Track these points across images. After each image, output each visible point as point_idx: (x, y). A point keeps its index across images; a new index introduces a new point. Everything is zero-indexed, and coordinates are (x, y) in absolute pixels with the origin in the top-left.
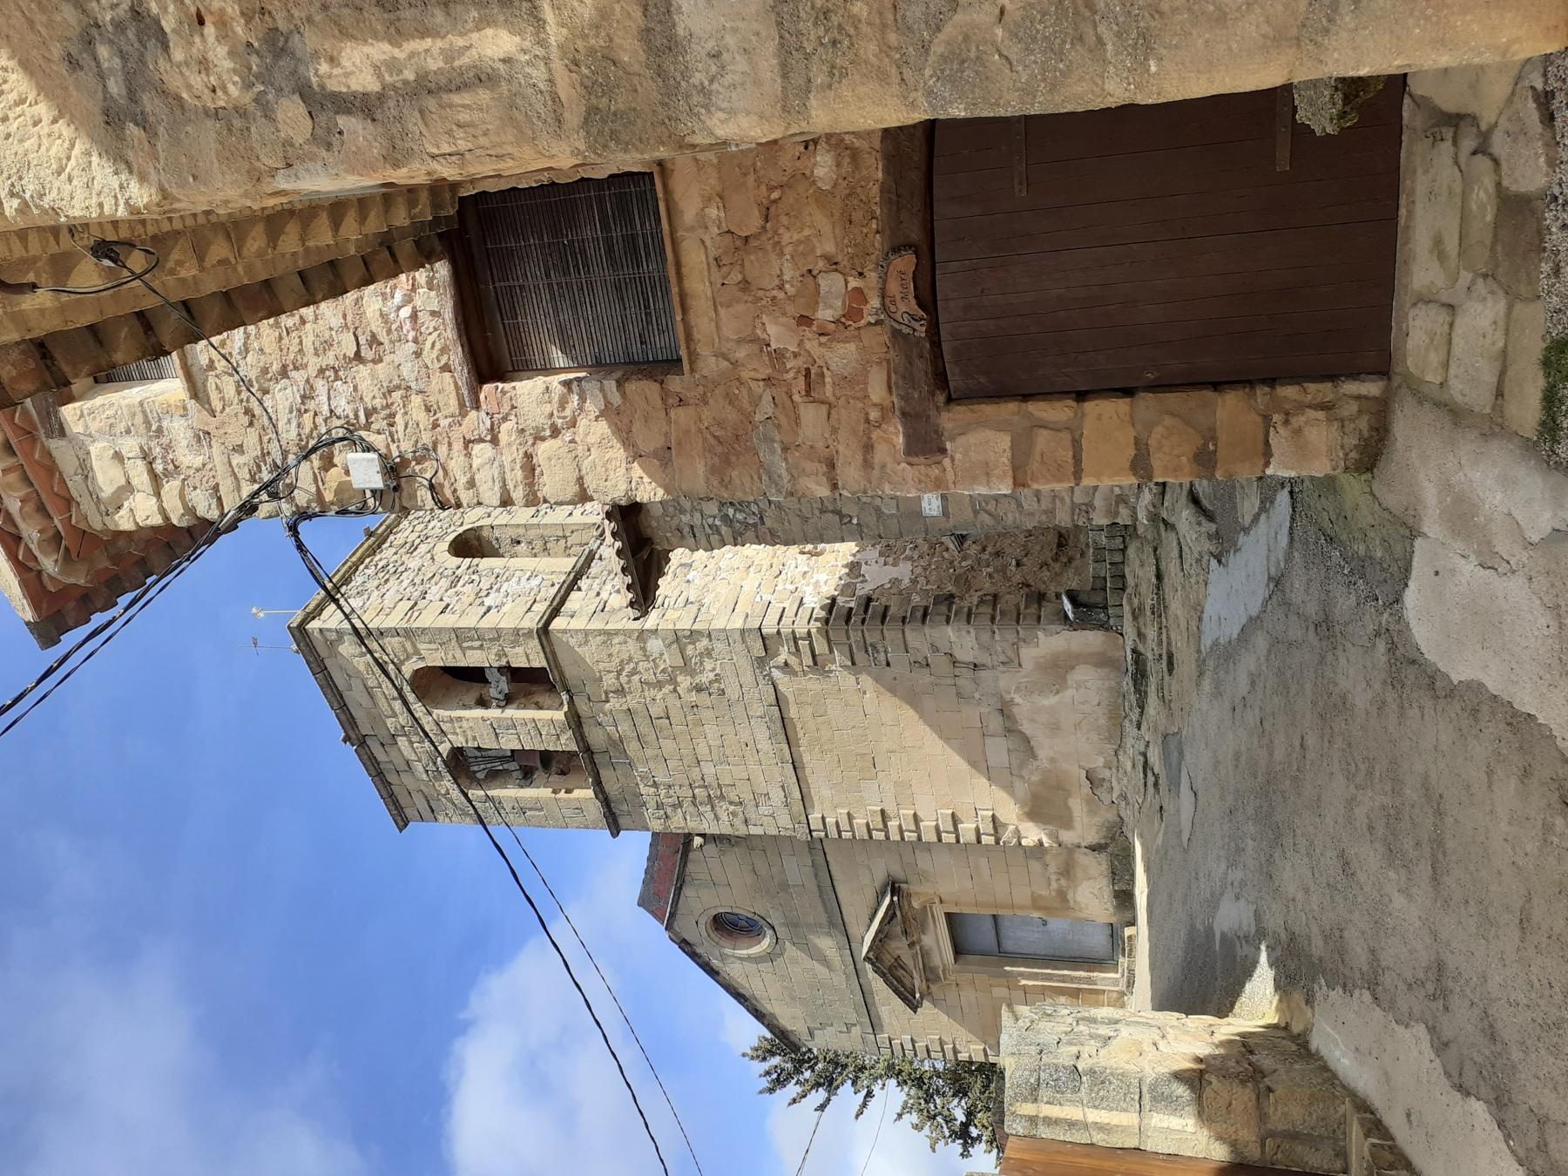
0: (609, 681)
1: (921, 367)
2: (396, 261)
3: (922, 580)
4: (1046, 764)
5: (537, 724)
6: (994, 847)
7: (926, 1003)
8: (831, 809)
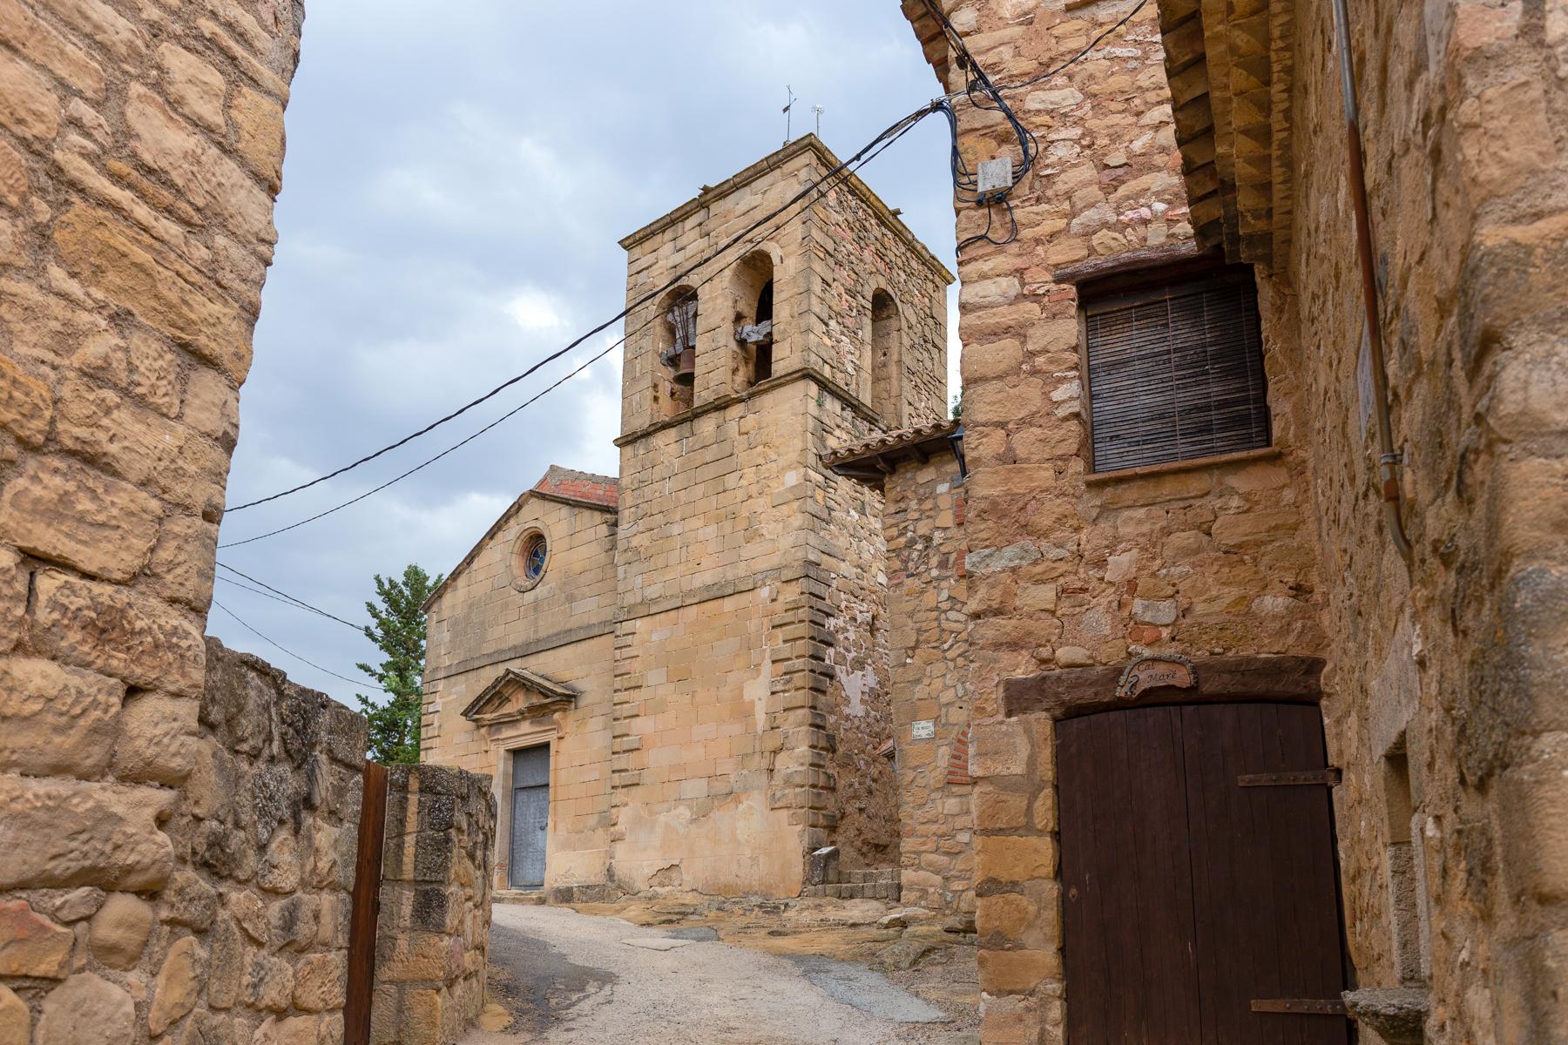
1: (1087, 695)
3: (848, 724)
5: (716, 366)
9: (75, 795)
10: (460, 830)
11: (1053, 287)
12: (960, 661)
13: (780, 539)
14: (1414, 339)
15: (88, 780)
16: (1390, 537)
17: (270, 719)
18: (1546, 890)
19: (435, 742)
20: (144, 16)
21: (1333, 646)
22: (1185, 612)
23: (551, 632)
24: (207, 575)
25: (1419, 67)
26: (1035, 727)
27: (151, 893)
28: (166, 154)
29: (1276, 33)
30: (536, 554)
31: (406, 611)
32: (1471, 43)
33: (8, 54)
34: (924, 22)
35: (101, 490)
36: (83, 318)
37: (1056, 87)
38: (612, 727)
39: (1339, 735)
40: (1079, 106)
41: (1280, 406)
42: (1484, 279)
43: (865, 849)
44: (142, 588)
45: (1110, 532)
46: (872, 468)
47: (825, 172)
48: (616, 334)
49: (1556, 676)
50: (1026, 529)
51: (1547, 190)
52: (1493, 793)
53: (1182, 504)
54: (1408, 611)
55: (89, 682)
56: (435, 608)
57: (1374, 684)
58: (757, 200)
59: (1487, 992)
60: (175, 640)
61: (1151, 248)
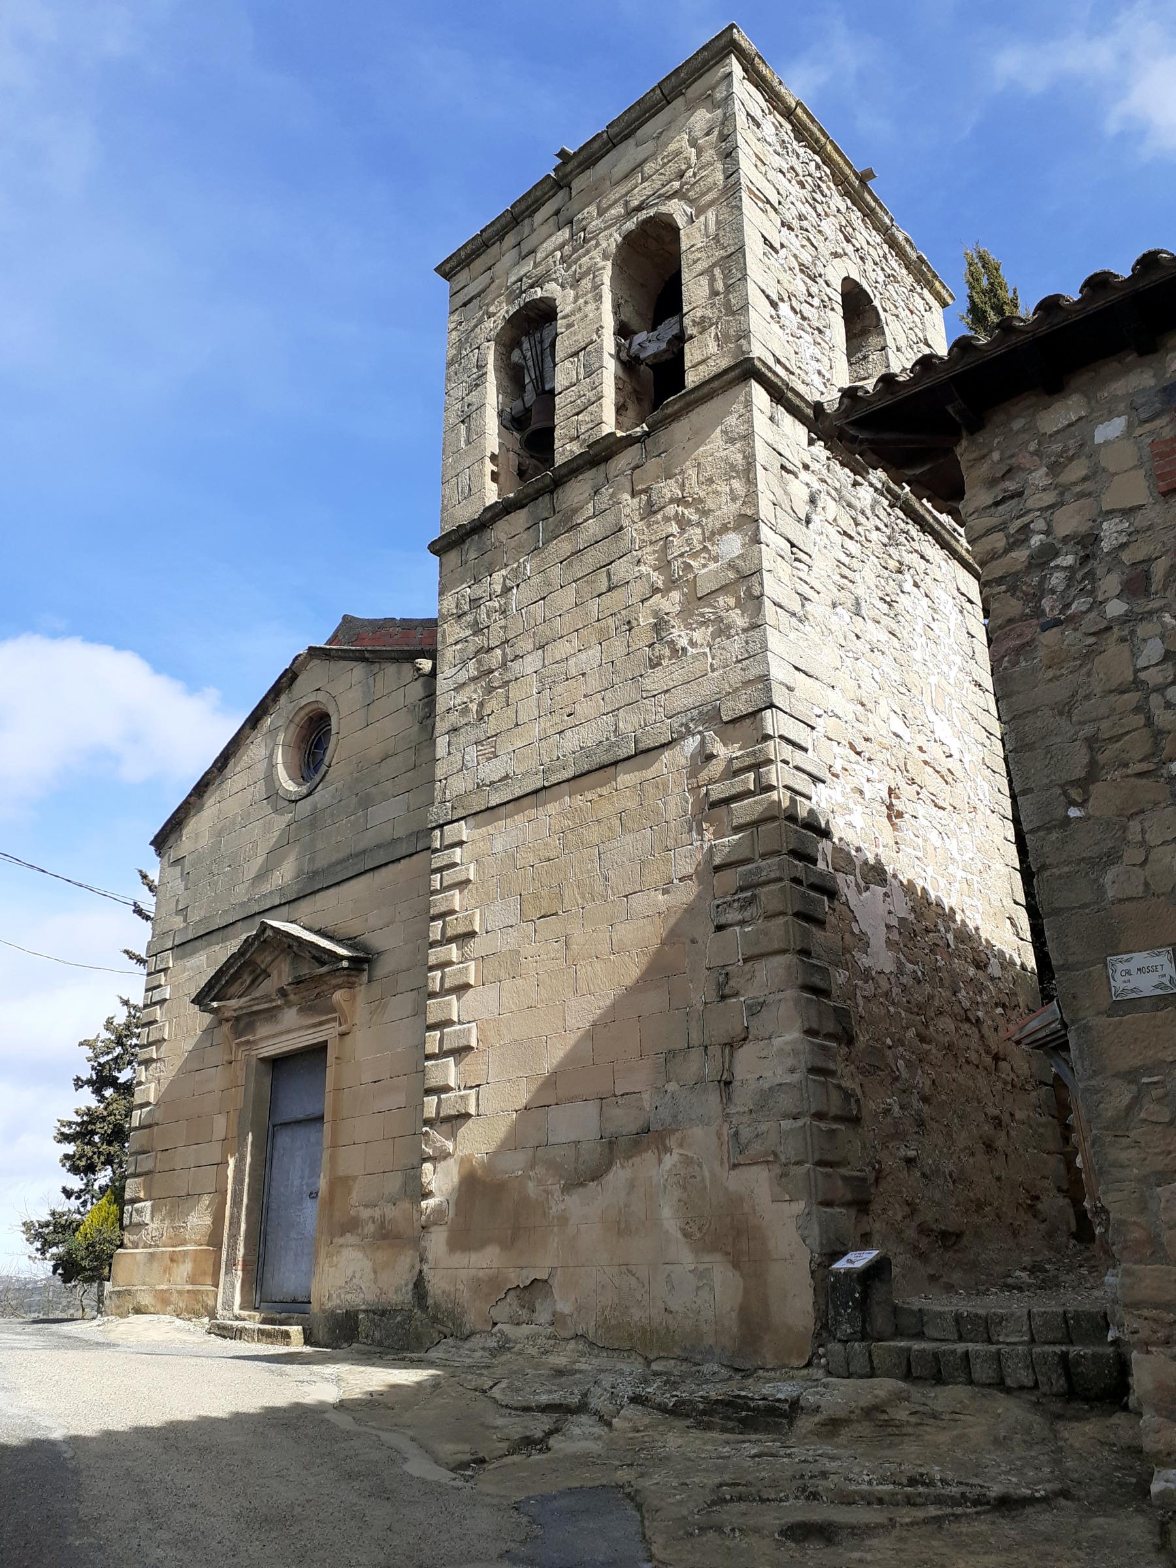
0: (668, 489)
4: (555, 1209)
5: (592, 396)
6: (423, 1122)
7: (208, 1018)
8: (472, 850)
43: (923, 1244)
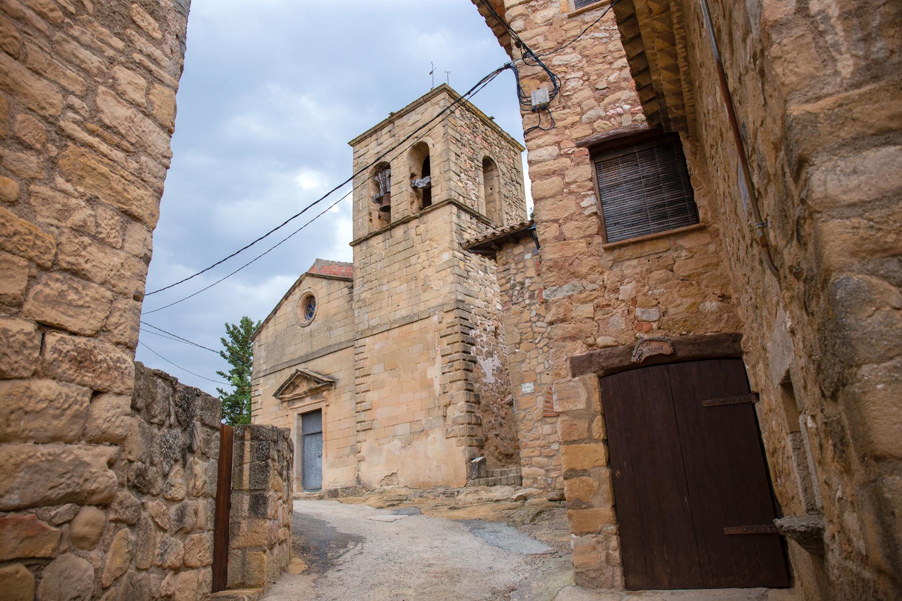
1: (616, 362)
2: (648, 102)
3: (486, 388)
5: (402, 200)
9: (63, 452)
10: (273, 460)
11: (576, 150)
12: (545, 349)
13: (442, 289)
14: (764, 164)
15: (71, 444)
16: (766, 266)
17: (169, 404)
18: (878, 453)
19: (259, 412)
20: (106, 54)
21: (746, 326)
22: (664, 314)
23: (320, 347)
24: (136, 329)
25: (747, 32)
26: (589, 382)
27: (104, 505)
28: (116, 118)
29: (675, 21)
30: (310, 306)
31: (242, 342)
32: (772, 18)
33: (37, 76)
34: (498, 27)
35: (80, 288)
36: (73, 202)
37: (567, 53)
38: (355, 398)
39: (755, 374)
40: (580, 61)
41: (701, 202)
42: (795, 131)
43: (500, 457)
44: (101, 338)
45: (619, 273)
46: (489, 248)
47: (453, 101)
48: (349, 187)
49: (864, 334)
50: (574, 275)
51: (822, 86)
52: (840, 401)
53: (656, 256)
54: (781, 304)
55: (72, 390)
56: (257, 339)
57: (769, 345)
58: (419, 117)
59: (855, 514)
60: (118, 364)
61: (624, 128)
